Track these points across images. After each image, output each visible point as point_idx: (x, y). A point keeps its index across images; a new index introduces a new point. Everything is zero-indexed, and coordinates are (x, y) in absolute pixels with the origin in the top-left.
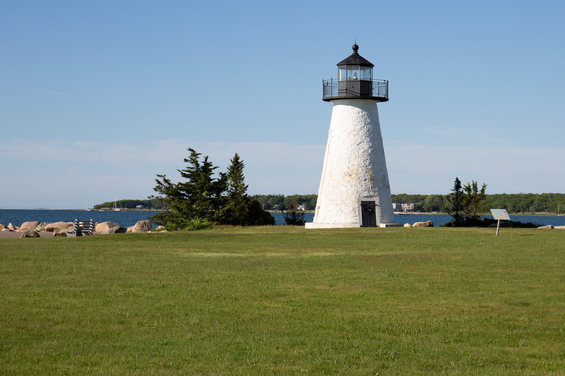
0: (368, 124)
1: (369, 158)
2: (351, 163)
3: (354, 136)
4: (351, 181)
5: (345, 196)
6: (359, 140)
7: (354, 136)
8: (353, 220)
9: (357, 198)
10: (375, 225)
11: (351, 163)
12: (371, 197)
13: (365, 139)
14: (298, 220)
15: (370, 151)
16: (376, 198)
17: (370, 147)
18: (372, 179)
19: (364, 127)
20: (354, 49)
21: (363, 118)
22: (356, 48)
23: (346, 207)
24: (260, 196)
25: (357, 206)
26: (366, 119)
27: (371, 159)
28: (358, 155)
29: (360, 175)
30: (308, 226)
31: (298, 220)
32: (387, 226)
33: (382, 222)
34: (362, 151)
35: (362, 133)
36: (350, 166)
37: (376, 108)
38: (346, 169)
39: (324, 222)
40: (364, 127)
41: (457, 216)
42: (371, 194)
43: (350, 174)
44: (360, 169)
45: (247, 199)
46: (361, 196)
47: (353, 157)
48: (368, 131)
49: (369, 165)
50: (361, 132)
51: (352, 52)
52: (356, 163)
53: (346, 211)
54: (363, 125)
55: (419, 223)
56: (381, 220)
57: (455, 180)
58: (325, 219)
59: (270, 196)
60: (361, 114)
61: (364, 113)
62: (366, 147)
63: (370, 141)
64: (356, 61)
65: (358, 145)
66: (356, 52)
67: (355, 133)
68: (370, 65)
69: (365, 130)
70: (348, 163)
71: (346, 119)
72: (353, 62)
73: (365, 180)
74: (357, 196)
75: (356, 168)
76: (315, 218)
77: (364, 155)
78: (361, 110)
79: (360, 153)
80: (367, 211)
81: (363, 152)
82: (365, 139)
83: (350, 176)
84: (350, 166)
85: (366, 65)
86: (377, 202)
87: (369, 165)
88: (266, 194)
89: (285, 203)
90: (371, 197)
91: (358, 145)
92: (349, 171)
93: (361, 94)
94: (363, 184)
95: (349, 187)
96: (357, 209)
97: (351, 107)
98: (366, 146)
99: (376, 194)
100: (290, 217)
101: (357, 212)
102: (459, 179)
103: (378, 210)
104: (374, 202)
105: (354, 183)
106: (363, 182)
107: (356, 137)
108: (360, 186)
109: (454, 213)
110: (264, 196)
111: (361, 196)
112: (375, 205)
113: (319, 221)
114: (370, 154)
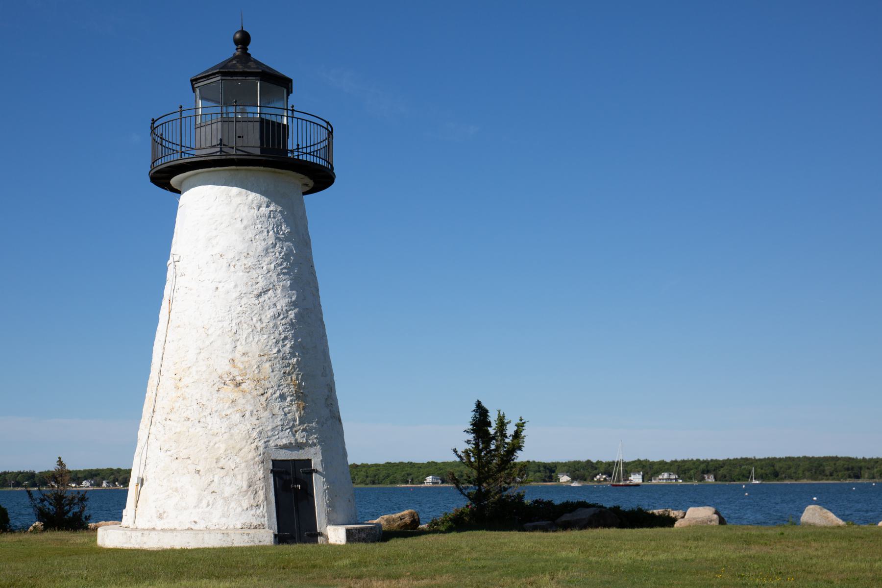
0: (286, 239)
1: (290, 334)
2: (240, 349)
3: (248, 270)
4: (241, 401)
5: (223, 447)
6: (262, 284)
7: (248, 270)
8: (250, 518)
9: (261, 450)
10: (313, 535)
11: (240, 349)
12: (300, 446)
13: (279, 280)
14: (70, 514)
15: (292, 314)
16: (312, 450)
17: (293, 304)
18: (300, 395)
19: (274, 246)
20: (237, 42)
21: (272, 220)
22: (244, 40)
23: (228, 480)
24: (8, 473)
25: (260, 474)
26: (279, 226)
27: (295, 337)
28: (259, 326)
29: (267, 384)
30: (109, 536)
31: (70, 514)
32: (349, 534)
33: (332, 522)
34: (270, 313)
35: (269, 263)
36: (237, 355)
37: (303, 200)
38: (224, 366)
39: (160, 525)
40: (274, 246)
41: (478, 498)
42: (300, 437)
43: (239, 379)
44: (267, 366)
45: (331, 545)
46: (272, 444)
47: (245, 332)
48: (286, 258)
49: (293, 355)
50: (267, 260)
51: (231, 50)
52: (255, 350)
53: (228, 491)
54: (271, 240)
55: (386, 517)
56: (328, 514)
57: (474, 407)
58: (160, 517)
59: (20, 473)
60: (264, 210)
61: (272, 208)
62: (282, 303)
63: (292, 287)
64: (245, 75)
65: (259, 296)
66: (245, 49)
67: (250, 262)
68: (284, 83)
69: (277, 254)
70: (229, 347)
71: (217, 226)
72: (240, 68)
73: (283, 397)
74: (261, 444)
75: (254, 363)
76: (128, 513)
77: (276, 326)
78: (265, 199)
79: (265, 321)
80: (290, 487)
81: (275, 317)
82: (279, 280)
83: (238, 385)
84: (237, 355)
85: (279, 83)
86: (316, 463)
87: (293, 355)
88: (15, 470)
89: (36, 479)
90: (300, 446)
91: (259, 296)
92: (235, 372)
93: (263, 150)
94: (276, 410)
95: (237, 417)
96: (261, 484)
97: (235, 190)
98: (280, 299)
99: (313, 438)
100: (50, 508)
101: (261, 494)
102: (485, 404)
103: (318, 485)
104: (309, 461)
105: (249, 408)
106: (277, 405)
107: (254, 274)
108: (267, 414)
109: (472, 489)
110: (13, 472)
111: (272, 444)
112: (311, 472)
113: (141, 523)
114: (292, 324)
